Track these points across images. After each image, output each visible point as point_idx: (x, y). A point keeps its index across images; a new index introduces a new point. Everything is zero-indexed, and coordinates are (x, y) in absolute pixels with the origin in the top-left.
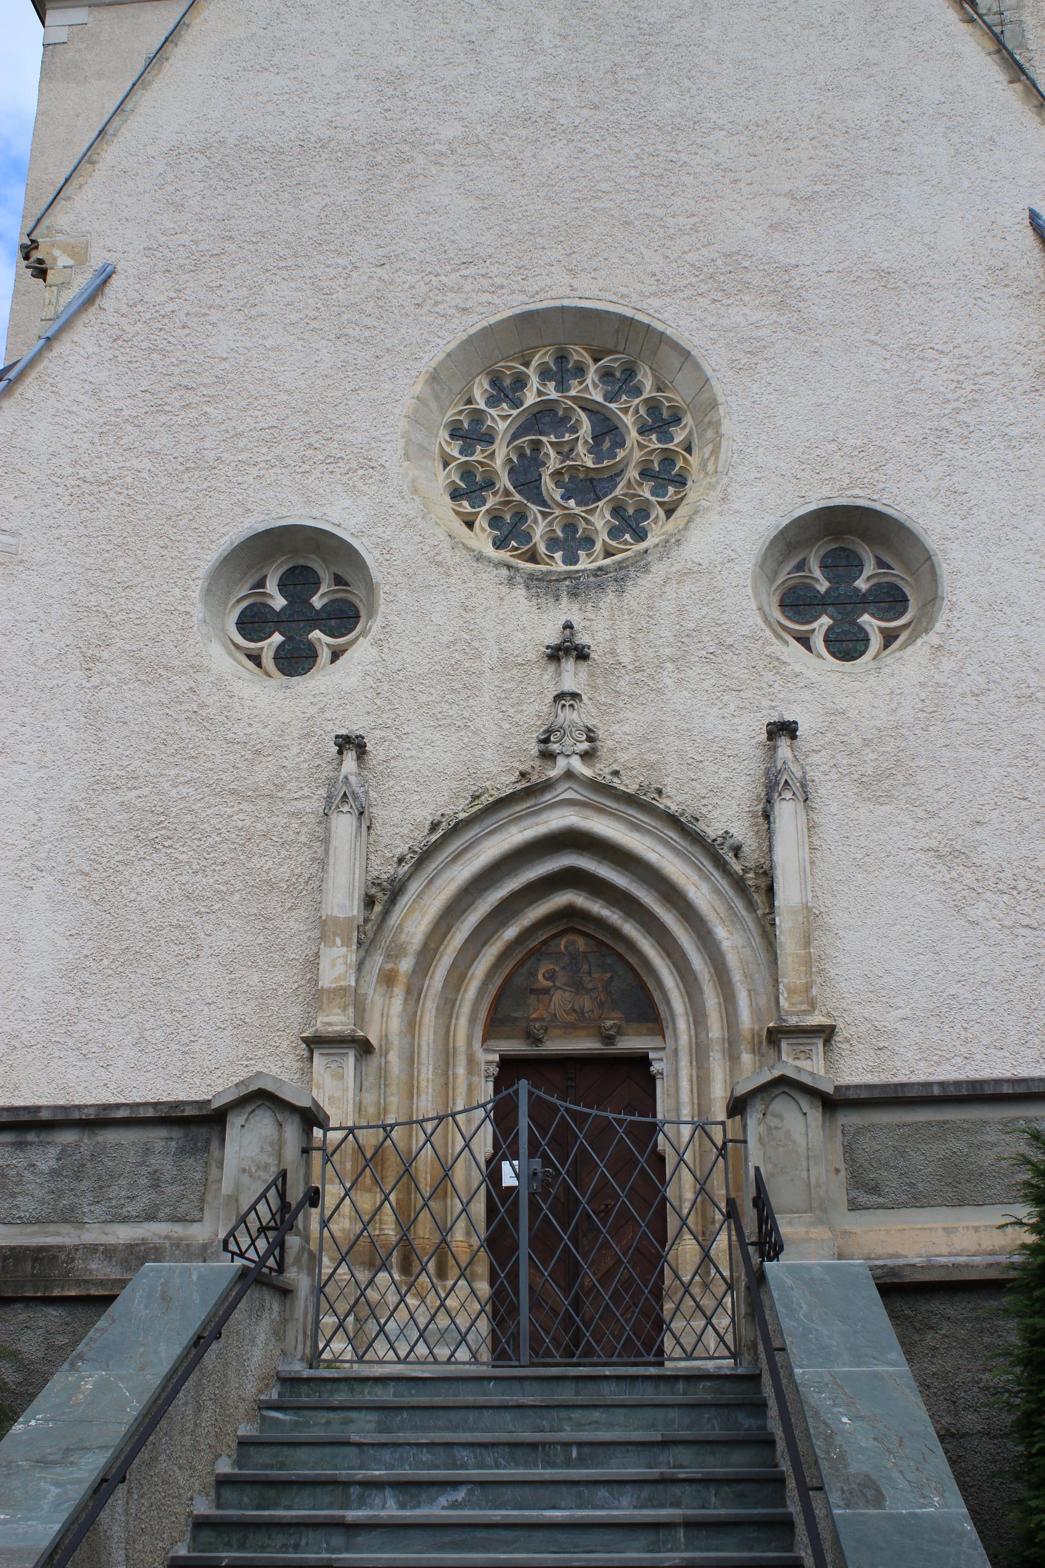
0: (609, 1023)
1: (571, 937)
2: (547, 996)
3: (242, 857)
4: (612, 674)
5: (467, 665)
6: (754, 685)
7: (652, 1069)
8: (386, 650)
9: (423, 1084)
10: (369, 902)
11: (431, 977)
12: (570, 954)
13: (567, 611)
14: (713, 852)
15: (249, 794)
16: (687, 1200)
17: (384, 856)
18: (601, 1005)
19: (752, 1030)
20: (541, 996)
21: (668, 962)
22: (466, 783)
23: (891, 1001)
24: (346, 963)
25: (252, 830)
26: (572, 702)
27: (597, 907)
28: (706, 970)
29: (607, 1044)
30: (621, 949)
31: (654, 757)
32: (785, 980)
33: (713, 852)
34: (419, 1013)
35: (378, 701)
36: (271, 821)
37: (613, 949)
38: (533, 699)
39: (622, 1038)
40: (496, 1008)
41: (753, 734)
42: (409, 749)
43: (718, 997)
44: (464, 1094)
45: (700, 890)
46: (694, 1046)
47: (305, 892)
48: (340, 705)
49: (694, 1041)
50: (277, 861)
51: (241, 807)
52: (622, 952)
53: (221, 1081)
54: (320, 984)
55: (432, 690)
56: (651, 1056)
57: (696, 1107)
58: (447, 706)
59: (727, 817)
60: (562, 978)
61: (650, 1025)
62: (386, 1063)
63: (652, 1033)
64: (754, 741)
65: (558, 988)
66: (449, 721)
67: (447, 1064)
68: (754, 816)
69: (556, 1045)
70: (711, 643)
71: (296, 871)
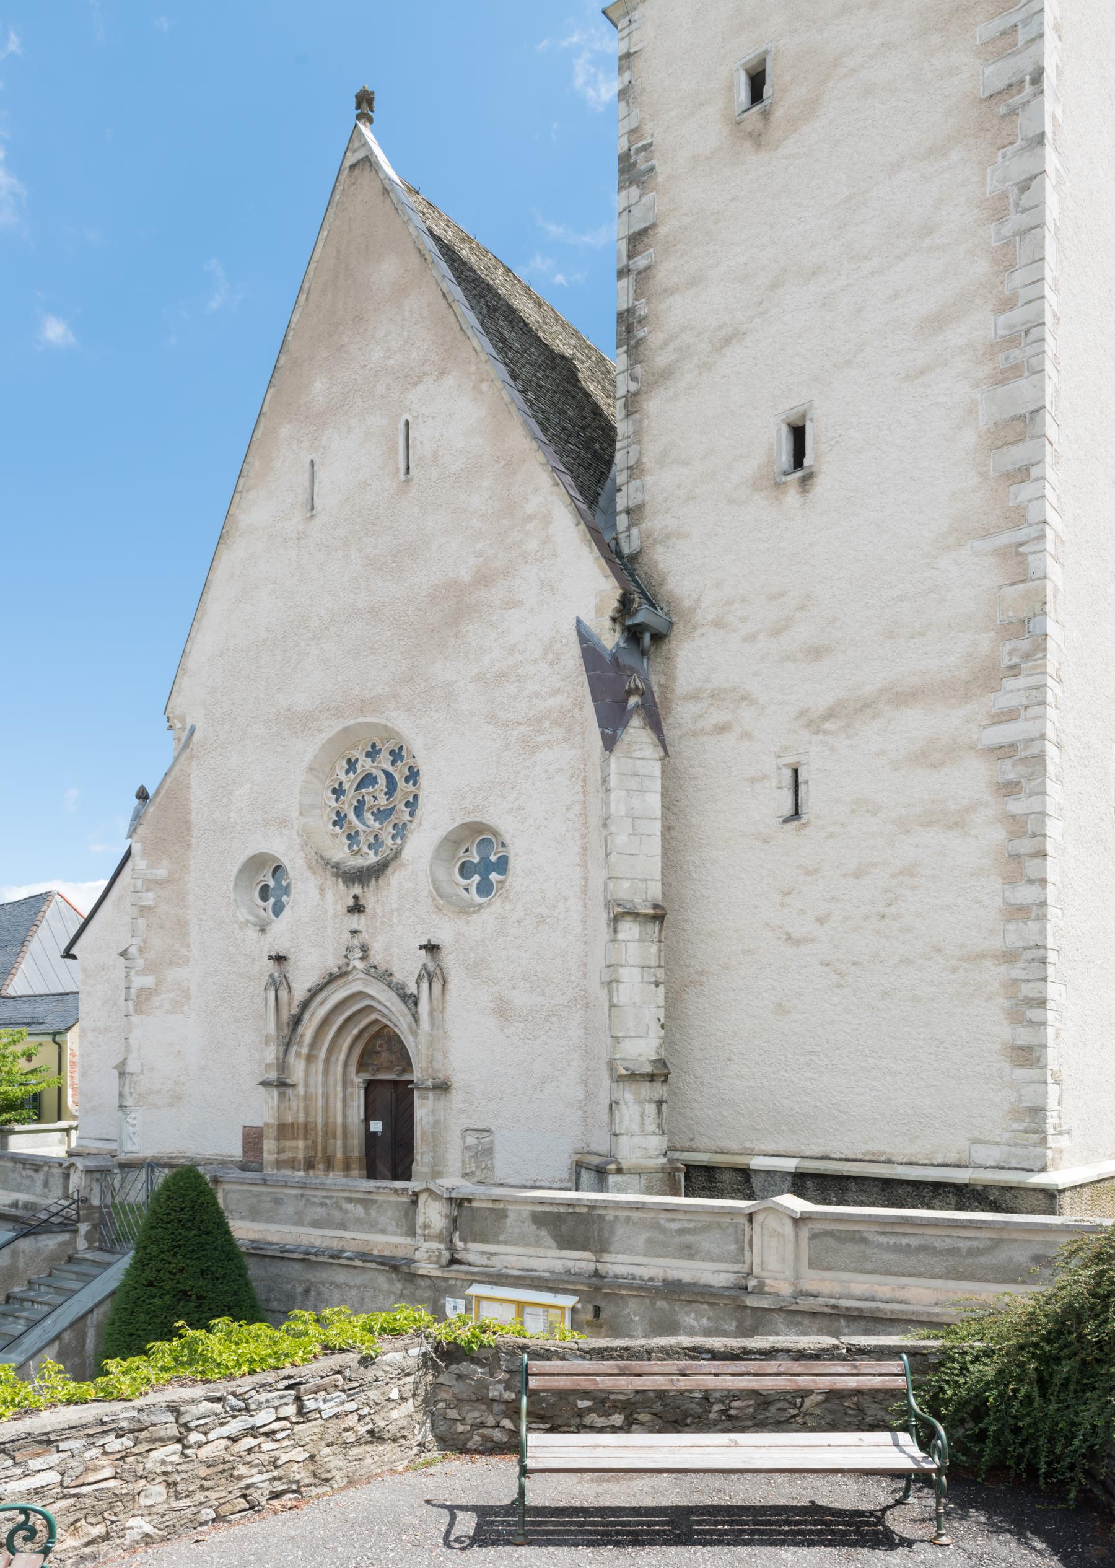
13: (357, 890)
60: (385, 1047)
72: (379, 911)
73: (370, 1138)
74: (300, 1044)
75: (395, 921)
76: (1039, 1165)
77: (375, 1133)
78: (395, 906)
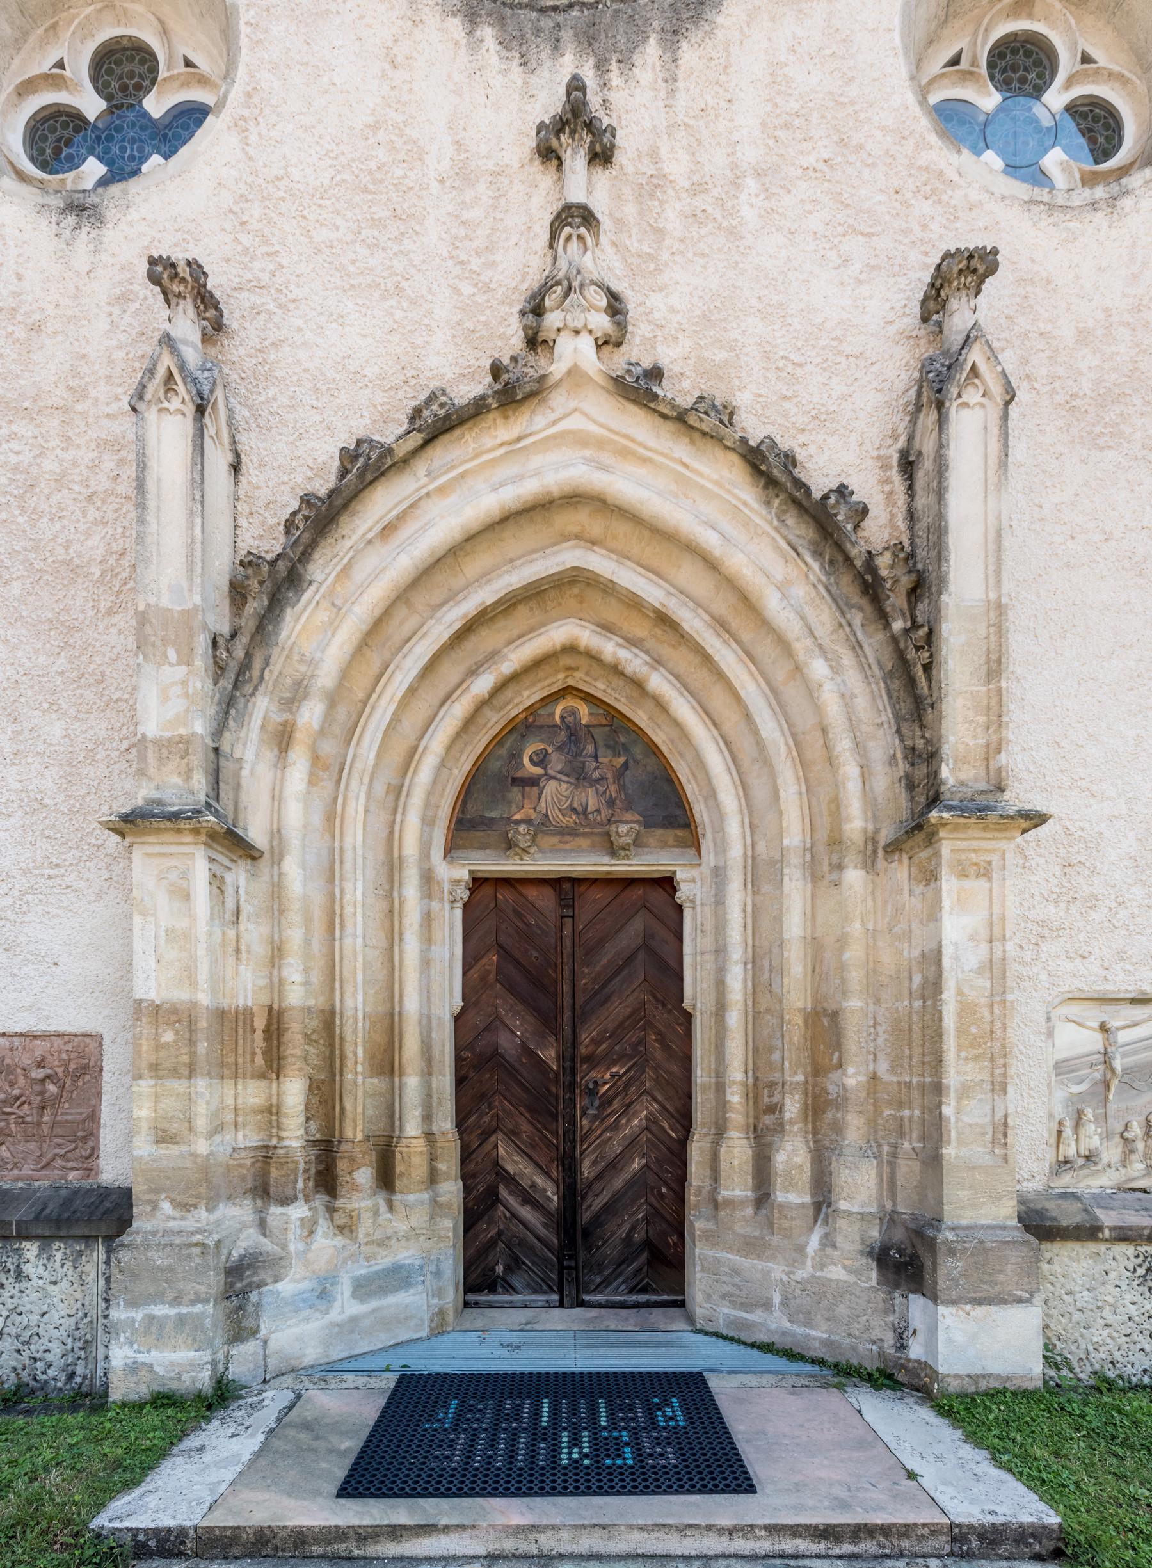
1: (569, 702)
2: (535, 789)
3: (21, 520)
4: (652, 196)
5: (399, 172)
7: (678, 894)
8: (253, 138)
9: (349, 910)
10: (238, 593)
12: (568, 727)
15: (26, 404)
16: (734, 1083)
17: (263, 523)
18: (611, 803)
19: (865, 831)
20: (527, 789)
22: (401, 394)
23: (1094, 788)
24: (187, 695)
25: (34, 471)
26: (583, 230)
28: (782, 741)
31: (720, 356)
34: (340, 800)
35: (245, 239)
36: (68, 456)
38: (514, 240)
41: (891, 316)
42: (299, 330)
44: (416, 926)
46: (750, 861)
49: (749, 854)
50: (82, 527)
51: (14, 428)
53: (10, 900)
54: (141, 729)
55: (339, 221)
57: (750, 950)
59: (845, 454)
60: (557, 762)
61: (679, 832)
62: (280, 875)
63: (682, 844)
64: (892, 330)
68: (885, 467)
71: (115, 547)
75: (749, 214)
76: (487, 890)
78: (749, 155)
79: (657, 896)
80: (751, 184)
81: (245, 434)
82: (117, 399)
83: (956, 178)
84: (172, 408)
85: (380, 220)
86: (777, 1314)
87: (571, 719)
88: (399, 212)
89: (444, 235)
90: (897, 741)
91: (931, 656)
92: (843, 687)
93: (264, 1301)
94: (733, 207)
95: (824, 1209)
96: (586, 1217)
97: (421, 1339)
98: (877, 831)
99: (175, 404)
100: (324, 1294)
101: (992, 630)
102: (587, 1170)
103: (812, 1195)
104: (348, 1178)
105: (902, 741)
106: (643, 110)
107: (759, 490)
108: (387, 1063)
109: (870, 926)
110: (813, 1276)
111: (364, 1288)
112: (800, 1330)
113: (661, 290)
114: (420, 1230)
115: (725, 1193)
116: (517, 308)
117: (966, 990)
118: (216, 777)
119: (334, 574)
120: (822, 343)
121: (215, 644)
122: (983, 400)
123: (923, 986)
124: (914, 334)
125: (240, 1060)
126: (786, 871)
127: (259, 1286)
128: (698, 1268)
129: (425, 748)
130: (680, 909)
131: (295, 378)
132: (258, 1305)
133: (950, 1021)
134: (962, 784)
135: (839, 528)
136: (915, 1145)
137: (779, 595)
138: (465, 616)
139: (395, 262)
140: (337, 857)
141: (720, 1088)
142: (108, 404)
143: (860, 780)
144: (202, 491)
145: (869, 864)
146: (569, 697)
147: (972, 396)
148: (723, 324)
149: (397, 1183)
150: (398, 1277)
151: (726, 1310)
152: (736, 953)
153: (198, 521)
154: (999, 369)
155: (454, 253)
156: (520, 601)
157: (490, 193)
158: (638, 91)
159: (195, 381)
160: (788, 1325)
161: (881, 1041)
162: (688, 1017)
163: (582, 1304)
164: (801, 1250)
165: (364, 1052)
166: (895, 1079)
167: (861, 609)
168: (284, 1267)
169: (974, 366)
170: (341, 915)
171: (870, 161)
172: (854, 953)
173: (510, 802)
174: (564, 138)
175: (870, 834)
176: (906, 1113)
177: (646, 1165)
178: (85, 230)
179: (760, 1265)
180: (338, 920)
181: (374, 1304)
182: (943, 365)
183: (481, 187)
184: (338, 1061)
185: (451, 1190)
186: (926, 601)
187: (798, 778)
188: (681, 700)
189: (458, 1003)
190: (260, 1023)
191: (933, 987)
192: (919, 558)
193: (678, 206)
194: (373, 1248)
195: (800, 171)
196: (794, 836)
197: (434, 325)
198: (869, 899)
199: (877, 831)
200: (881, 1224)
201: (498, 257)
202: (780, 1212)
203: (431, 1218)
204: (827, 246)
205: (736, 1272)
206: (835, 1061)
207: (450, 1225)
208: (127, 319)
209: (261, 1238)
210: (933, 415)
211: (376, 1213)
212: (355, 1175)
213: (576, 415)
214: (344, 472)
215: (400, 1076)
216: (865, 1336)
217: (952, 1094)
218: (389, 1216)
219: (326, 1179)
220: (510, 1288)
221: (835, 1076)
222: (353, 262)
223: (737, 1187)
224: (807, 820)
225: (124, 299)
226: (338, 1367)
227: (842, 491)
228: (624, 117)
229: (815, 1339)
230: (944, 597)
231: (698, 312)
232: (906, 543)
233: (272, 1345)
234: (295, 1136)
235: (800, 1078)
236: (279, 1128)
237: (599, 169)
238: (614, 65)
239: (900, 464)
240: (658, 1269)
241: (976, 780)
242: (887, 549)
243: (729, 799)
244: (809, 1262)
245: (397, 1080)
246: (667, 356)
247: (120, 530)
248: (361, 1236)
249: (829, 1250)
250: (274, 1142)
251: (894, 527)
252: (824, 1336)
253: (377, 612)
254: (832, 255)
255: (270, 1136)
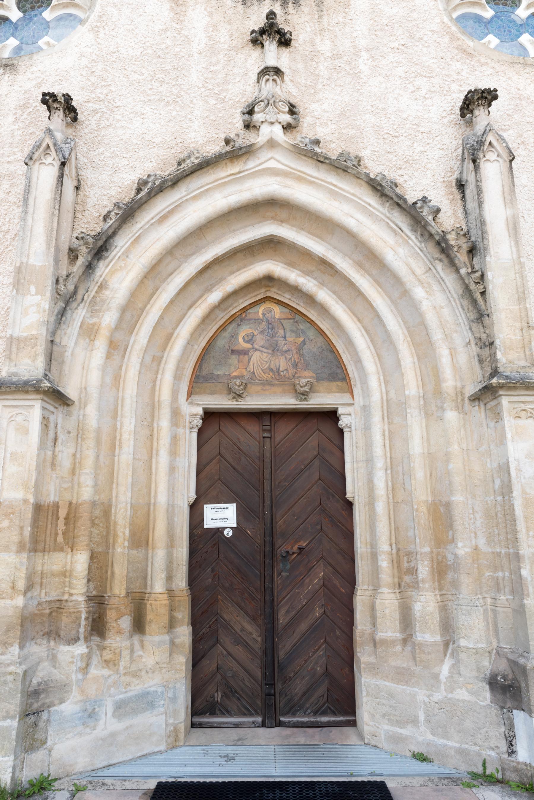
0: (303, 381)
1: (268, 305)
2: (246, 356)
4: (312, 60)
5: (177, 50)
6: (443, 73)
7: (340, 423)
8: (101, 35)
9: (125, 436)
11: (137, 334)
12: (268, 321)
14: (417, 216)
18: (295, 365)
19: (456, 388)
20: (241, 357)
21: (360, 325)
26: (275, 77)
27: (293, 276)
29: (301, 400)
30: (312, 315)
31: (352, 132)
32: (501, 336)
33: (417, 216)
34: (124, 368)
37: (305, 316)
38: (238, 80)
39: (314, 395)
40: (200, 367)
41: (444, 114)
42: (119, 120)
43: (413, 357)
44: (167, 446)
45: (401, 251)
47: (10, 248)
48: (55, 82)
49: (385, 398)
52: (313, 319)
56: (340, 411)
57: (388, 460)
58: (157, 84)
59: (427, 180)
60: (260, 341)
61: (339, 383)
62: (84, 415)
63: (341, 390)
64: (446, 120)
65: (256, 350)
66: (159, 97)
67: (153, 416)
69: (254, 401)
70: (402, 37)
72: (325, 46)
73: (202, 541)
74: (95, 307)
77: (219, 531)
79: (326, 427)
80: (365, 55)
81: (85, 171)
82: (14, 153)
83: (472, 52)
84: (47, 163)
85: (166, 70)
86: (422, 728)
87: (269, 315)
88: (176, 67)
89: (200, 77)
90: (470, 334)
91: (485, 288)
92: (436, 297)
93: (52, 718)
94: (355, 65)
95: (451, 646)
96: (282, 654)
97: (160, 752)
98: (463, 387)
99: (49, 160)
100: (90, 715)
101: (517, 275)
102: (282, 619)
103: (442, 635)
104: (114, 624)
105: (473, 334)
106: (306, 23)
107: (377, 198)
108: (141, 539)
109: (464, 446)
110: (446, 697)
111: (122, 708)
112: (442, 741)
113: (318, 101)
114: (160, 664)
115: (380, 635)
116: (239, 110)
117: (528, 491)
118: (50, 358)
119: (130, 241)
120: (408, 126)
121: (57, 281)
122: (498, 159)
123: (502, 487)
124: (458, 122)
125: (48, 539)
126: (408, 410)
127: (49, 707)
128: (364, 693)
129: (178, 334)
130: (341, 432)
131: (115, 143)
132: (48, 721)
133: (519, 511)
134: (510, 362)
135: (424, 219)
136: (508, 597)
137: (393, 253)
138: (206, 261)
139: (173, 89)
140: (120, 403)
141: (374, 556)
142: (9, 156)
143: (449, 357)
144: (60, 204)
145: (459, 408)
146: (267, 302)
147: (491, 156)
148: (353, 118)
149: (147, 628)
150: (145, 702)
151: (386, 727)
152: (380, 464)
153: (56, 219)
154: (504, 145)
155: (206, 85)
156: (238, 252)
157: (225, 59)
158: (303, 15)
159: (61, 150)
160: (431, 737)
161: (478, 523)
162: (350, 505)
163: (280, 724)
164: (436, 677)
165: (130, 531)
166: (490, 550)
167: (441, 260)
168: (67, 692)
169: (490, 143)
170: (120, 440)
171: (426, 45)
172: (456, 465)
173: (230, 365)
174: (264, 37)
175: (459, 389)
176: (500, 574)
177: (324, 613)
178: (7, 76)
179: (409, 690)
180: (117, 443)
181: (127, 722)
182: (474, 141)
183: (221, 56)
184: (112, 538)
185: (184, 634)
186: (479, 257)
187: (412, 354)
188: (337, 306)
189: (193, 496)
190: (62, 513)
191: (507, 489)
192: (472, 234)
193: (326, 64)
194: (127, 679)
195: (390, 49)
196: (413, 389)
197: (193, 118)
198: (462, 430)
199: (463, 387)
200: (490, 657)
201: (230, 87)
202: (419, 648)
203: (170, 655)
204: (407, 82)
205: (391, 696)
206: (450, 537)
207: (182, 661)
208: (25, 116)
209: (52, 669)
210: (471, 165)
211: (132, 651)
212: (120, 622)
213: (272, 160)
214: (139, 191)
215: (153, 549)
216: (486, 744)
217: (527, 561)
218: (141, 653)
219: (98, 626)
220: (226, 712)
221: (450, 547)
222: (150, 89)
223: (389, 630)
224: (419, 379)
225: (23, 107)
226: (100, 773)
227: (424, 200)
228: (296, 26)
229: (451, 748)
230: (488, 259)
231: (339, 112)
232: (464, 227)
233: (54, 753)
234: (78, 592)
235: (427, 549)
236: (70, 587)
237: (284, 49)
238: (290, 5)
239: (456, 185)
240: (340, 703)
241: (519, 359)
242: (453, 230)
243: (370, 364)
244: (442, 687)
245: (150, 551)
246: (321, 133)
247: (7, 220)
248: (121, 668)
249: (456, 676)
250: (66, 597)
251: (457, 217)
252: (457, 745)
253: (154, 262)
254: (410, 86)
255: (63, 593)
